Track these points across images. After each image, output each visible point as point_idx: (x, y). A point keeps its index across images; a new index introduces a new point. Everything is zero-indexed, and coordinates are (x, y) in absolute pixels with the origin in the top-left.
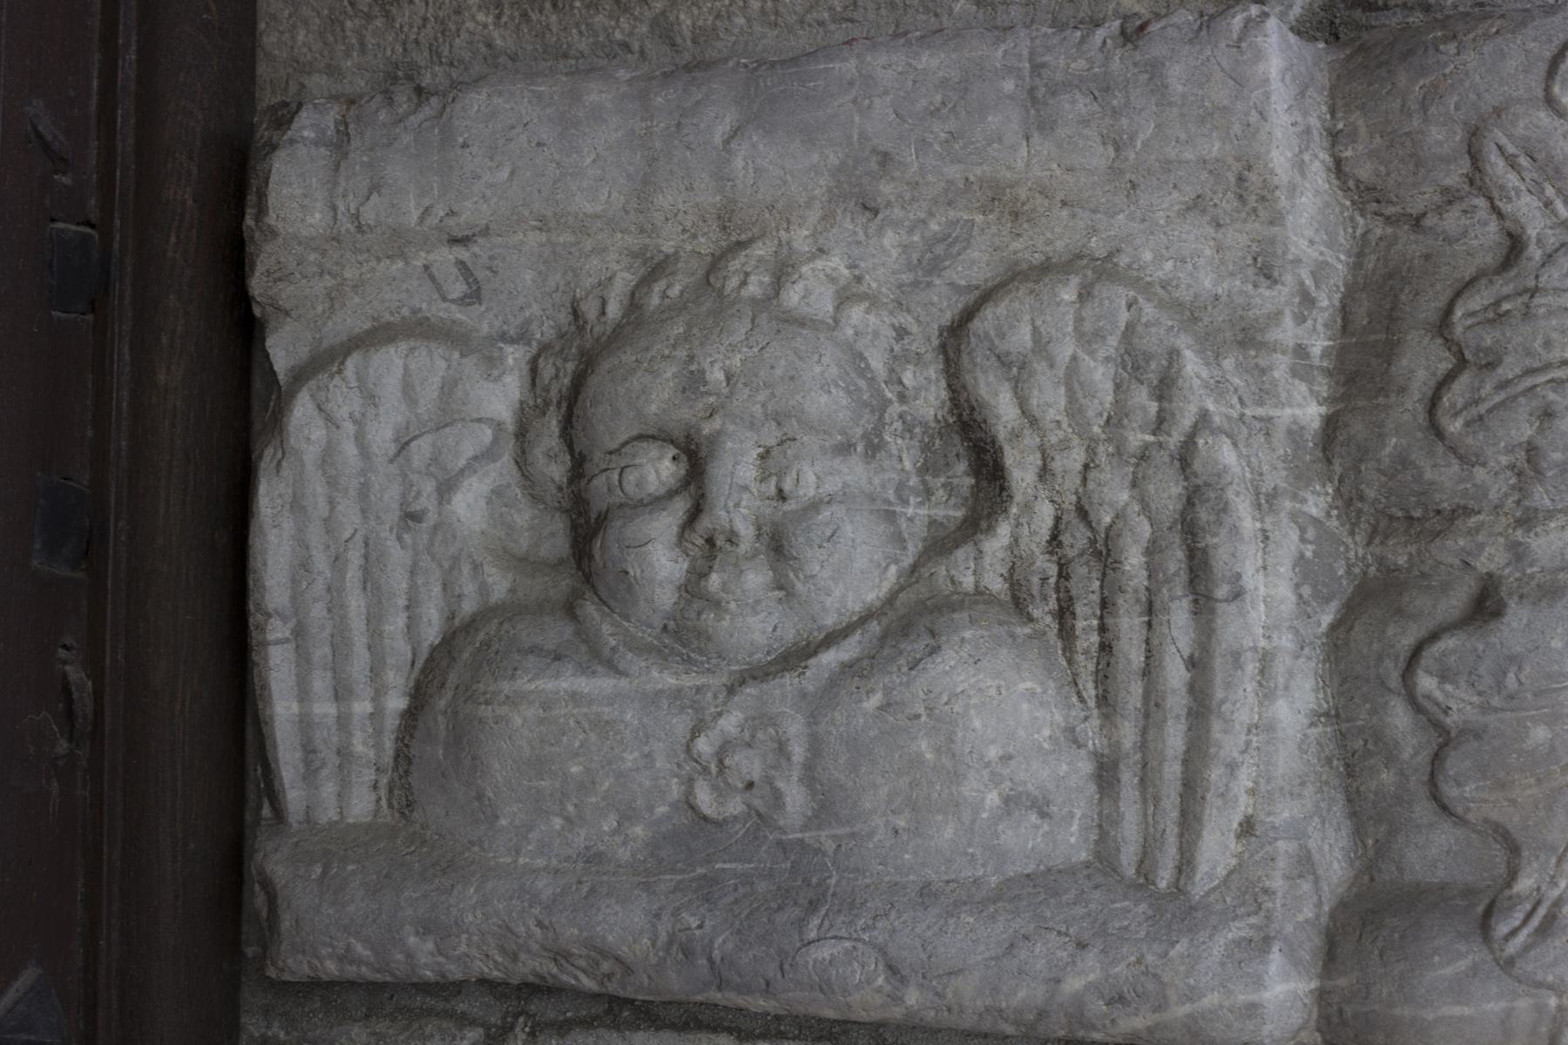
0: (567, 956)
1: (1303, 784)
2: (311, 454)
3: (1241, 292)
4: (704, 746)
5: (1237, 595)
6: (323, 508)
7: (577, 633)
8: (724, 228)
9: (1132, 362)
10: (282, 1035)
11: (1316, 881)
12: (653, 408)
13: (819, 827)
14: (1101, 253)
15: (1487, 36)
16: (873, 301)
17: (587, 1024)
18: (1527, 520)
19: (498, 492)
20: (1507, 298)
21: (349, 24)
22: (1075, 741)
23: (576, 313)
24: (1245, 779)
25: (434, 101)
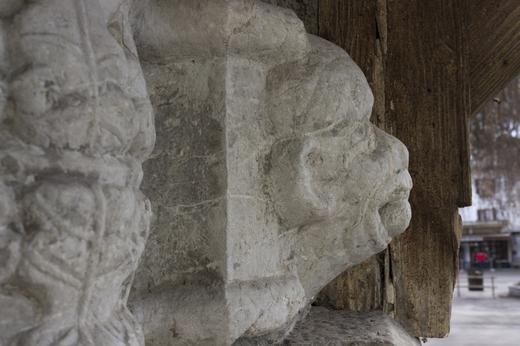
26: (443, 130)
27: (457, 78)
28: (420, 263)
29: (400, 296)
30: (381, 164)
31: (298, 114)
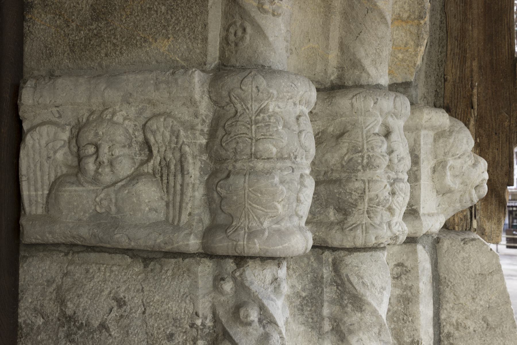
0: (75, 238)
1: (201, 207)
2: (30, 146)
3: (192, 120)
4: (97, 199)
5: (188, 173)
6: (32, 156)
7: (77, 179)
8: (104, 106)
9: (172, 132)
10: (27, 255)
11: (203, 224)
12: (90, 139)
13: (118, 214)
14: (169, 112)
15: (232, 76)
16: (130, 120)
17: (82, 252)
18: (236, 161)
19: (65, 153)
20: (233, 122)
21: (41, 61)
22: (162, 199)
23: (78, 120)
24: (189, 205)
25: (52, 80)
26: (502, 152)
27: (509, 128)
28: (489, 211)
29: (479, 225)
30: (476, 169)
31: (446, 151)
